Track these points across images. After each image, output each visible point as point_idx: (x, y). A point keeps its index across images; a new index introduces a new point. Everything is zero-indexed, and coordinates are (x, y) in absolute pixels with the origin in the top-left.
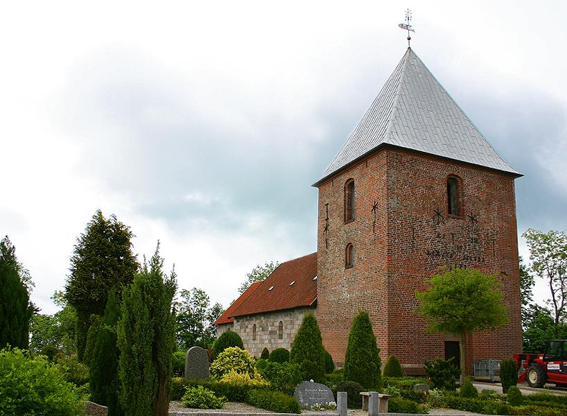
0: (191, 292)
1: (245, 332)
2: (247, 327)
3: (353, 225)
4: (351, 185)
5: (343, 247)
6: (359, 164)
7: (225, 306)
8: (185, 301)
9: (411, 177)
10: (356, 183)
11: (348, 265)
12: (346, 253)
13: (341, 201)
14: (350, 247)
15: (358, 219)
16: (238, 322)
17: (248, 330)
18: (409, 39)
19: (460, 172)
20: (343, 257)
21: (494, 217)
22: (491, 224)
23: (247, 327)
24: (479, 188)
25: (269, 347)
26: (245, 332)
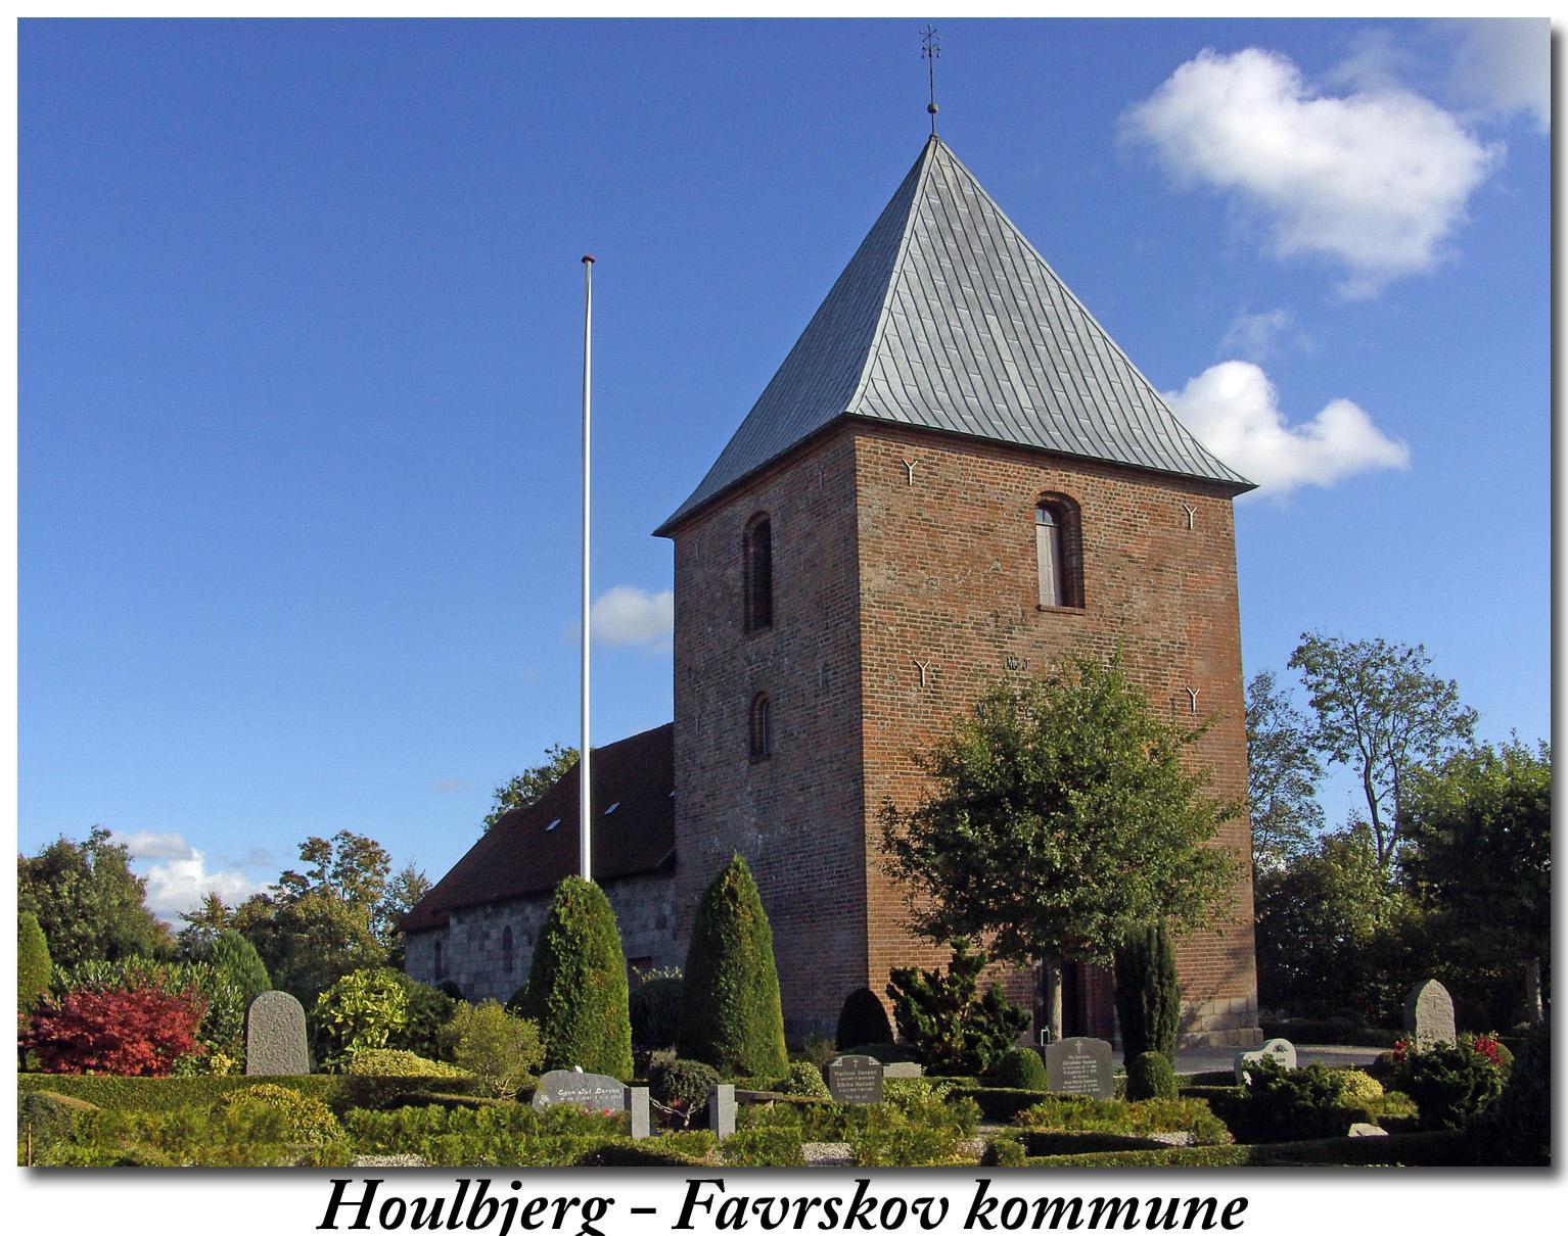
0: (335, 845)
1: (482, 948)
2: (487, 936)
3: (765, 641)
4: (761, 532)
5: (744, 701)
6: (782, 471)
7: (434, 878)
8: (316, 868)
9: (930, 506)
10: (775, 525)
11: (758, 751)
12: (752, 718)
13: (734, 574)
14: (760, 703)
15: (782, 626)
16: (460, 921)
17: (488, 944)
18: (931, 110)
19: (1074, 484)
20: (743, 732)
21: (1171, 606)
22: (1165, 624)
23: (487, 936)
24: (1129, 527)
25: (1231, 942)
26: (482, 948)
